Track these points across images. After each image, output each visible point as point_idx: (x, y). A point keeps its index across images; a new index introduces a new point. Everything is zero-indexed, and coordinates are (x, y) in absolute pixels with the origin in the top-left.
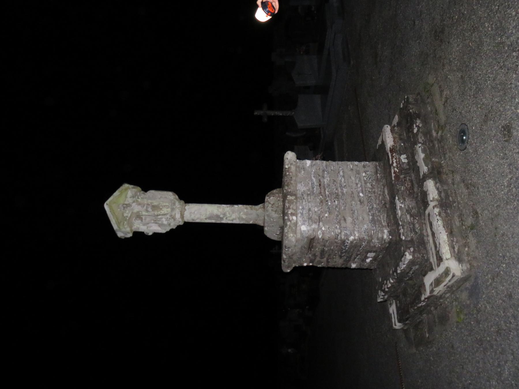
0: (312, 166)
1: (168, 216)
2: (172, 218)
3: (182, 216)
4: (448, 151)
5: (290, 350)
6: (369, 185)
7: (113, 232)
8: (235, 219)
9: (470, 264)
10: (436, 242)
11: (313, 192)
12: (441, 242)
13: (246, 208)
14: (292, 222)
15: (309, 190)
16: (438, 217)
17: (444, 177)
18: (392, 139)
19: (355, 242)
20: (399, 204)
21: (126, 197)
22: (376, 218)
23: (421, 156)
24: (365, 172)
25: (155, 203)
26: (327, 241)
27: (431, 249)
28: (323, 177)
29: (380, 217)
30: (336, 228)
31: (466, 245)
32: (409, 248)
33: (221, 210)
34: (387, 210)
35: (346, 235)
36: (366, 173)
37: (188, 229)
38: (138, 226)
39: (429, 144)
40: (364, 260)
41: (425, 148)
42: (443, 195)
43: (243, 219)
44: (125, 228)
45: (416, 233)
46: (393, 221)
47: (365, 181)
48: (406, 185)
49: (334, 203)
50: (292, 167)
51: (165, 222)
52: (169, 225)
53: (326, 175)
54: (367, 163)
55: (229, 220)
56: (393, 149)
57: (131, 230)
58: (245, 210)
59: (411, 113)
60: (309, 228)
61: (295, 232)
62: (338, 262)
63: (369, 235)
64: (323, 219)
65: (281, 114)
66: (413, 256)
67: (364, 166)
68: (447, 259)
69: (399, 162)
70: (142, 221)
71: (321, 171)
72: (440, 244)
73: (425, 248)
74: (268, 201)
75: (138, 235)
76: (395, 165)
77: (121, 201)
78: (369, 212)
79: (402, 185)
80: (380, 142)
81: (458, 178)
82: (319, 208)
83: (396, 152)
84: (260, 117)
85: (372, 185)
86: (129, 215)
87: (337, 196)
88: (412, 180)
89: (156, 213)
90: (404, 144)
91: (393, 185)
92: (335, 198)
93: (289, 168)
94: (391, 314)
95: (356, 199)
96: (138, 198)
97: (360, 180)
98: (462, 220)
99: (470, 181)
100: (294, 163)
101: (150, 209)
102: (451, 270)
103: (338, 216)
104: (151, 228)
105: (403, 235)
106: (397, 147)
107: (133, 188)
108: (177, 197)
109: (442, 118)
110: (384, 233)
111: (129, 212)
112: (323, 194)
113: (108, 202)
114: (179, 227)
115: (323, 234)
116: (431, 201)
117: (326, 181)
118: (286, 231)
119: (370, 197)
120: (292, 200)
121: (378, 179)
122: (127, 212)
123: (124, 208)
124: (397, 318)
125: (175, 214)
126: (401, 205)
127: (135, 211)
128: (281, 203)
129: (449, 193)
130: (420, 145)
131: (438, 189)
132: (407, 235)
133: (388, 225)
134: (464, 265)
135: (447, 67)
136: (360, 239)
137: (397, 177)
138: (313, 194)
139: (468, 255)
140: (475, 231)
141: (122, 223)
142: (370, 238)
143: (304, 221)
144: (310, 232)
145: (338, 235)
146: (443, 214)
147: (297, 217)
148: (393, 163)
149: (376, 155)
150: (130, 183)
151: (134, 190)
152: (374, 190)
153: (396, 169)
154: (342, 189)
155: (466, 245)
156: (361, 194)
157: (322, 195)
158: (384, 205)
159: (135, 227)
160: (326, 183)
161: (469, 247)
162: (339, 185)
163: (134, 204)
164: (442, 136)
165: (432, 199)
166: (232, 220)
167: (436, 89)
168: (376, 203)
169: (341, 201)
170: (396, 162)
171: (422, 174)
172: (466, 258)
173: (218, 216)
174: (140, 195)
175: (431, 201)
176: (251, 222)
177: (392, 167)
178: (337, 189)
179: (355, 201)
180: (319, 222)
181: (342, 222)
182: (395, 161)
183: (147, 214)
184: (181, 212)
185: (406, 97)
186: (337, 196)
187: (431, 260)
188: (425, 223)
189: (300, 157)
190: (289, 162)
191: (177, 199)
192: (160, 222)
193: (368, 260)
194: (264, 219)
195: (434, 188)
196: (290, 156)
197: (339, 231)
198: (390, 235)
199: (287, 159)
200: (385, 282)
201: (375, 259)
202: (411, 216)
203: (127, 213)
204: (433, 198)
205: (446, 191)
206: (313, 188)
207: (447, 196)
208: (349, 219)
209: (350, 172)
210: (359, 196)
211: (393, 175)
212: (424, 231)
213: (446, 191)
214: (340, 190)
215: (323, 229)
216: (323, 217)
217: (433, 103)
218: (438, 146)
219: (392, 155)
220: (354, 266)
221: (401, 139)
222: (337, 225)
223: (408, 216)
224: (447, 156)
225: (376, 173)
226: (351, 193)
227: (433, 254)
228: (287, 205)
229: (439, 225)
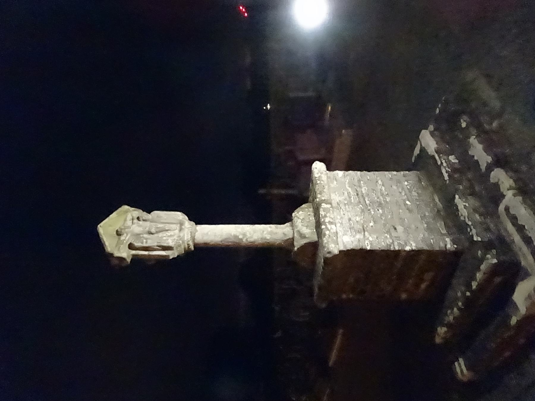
0: (344, 176)
1: (175, 237)
6: (414, 194)
14: (332, 231)
15: (345, 199)
28: (360, 187)
36: (408, 182)
37: (201, 253)
50: (322, 175)
54: (407, 172)
60: (353, 239)
67: (404, 176)
69: (448, 162)
76: (445, 164)
80: (417, 151)
87: (380, 205)
93: (319, 176)
115: (371, 244)
118: (326, 241)
120: (328, 208)
125: (184, 235)
126: (464, 204)
148: (442, 163)
153: (447, 169)
156: (408, 202)
160: (364, 192)
162: (379, 194)
170: (446, 162)
171: (483, 167)
177: (442, 167)
180: (364, 232)
181: (392, 230)
182: (444, 161)
189: (330, 168)
190: (319, 171)
196: (318, 167)
197: (391, 241)
198: (454, 244)
202: (480, 215)
204: (510, 186)
206: (350, 197)
208: (400, 229)
210: (406, 204)
215: (371, 239)
216: (367, 226)
222: (386, 235)
225: (420, 180)
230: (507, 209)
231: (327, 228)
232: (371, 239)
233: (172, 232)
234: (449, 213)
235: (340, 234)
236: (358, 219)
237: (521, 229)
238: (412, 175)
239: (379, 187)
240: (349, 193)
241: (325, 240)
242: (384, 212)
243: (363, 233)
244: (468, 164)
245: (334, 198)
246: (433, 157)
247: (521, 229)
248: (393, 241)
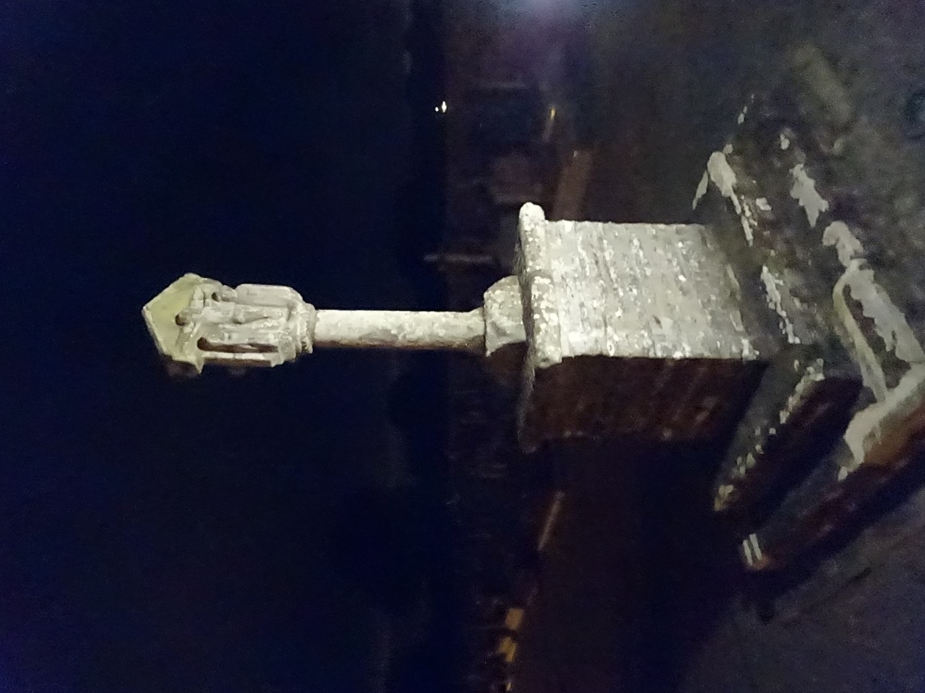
15: (576, 271)
28: (602, 250)
30: (643, 336)
37: (325, 358)
47: (684, 256)
49: (630, 293)
60: (585, 338)
64: (613, 321)
66: (825, 375)
76: (748, 214)
80: (702, 190)
85: (699, 262)
87: (635, 281)
93: (532, 230)
97: (675, 254)
113: (149, 304)
115: (617, 347)
133: (747, 331)
138: (586, 277)
148: (743, 212)
153: (752, 221)
154: (642, 269)
160: (608, 258)
162: (634, 262)
173: (386, 331)
180: (606, 326)
181: (653, 324)
182: (746, 208)
190: (532, 221)
197: (650, 343)
198: (755, 348)
202: (802, 301)
206: (583, 268)
208: (666, 322)
210: (678, 282)
216: (611, 317)
219: (739, 199)
222: (643, 332)
223: (797, 302)
230: (847, 290)
232: (616, 338)
233: (276, 321)
235: (564, 329)
240: (582, 260)
241: (539, 339)
242: (640, 293)
243: (603, 328)
244: (787, 213)
246: (729, 201)
247: (866, 325)
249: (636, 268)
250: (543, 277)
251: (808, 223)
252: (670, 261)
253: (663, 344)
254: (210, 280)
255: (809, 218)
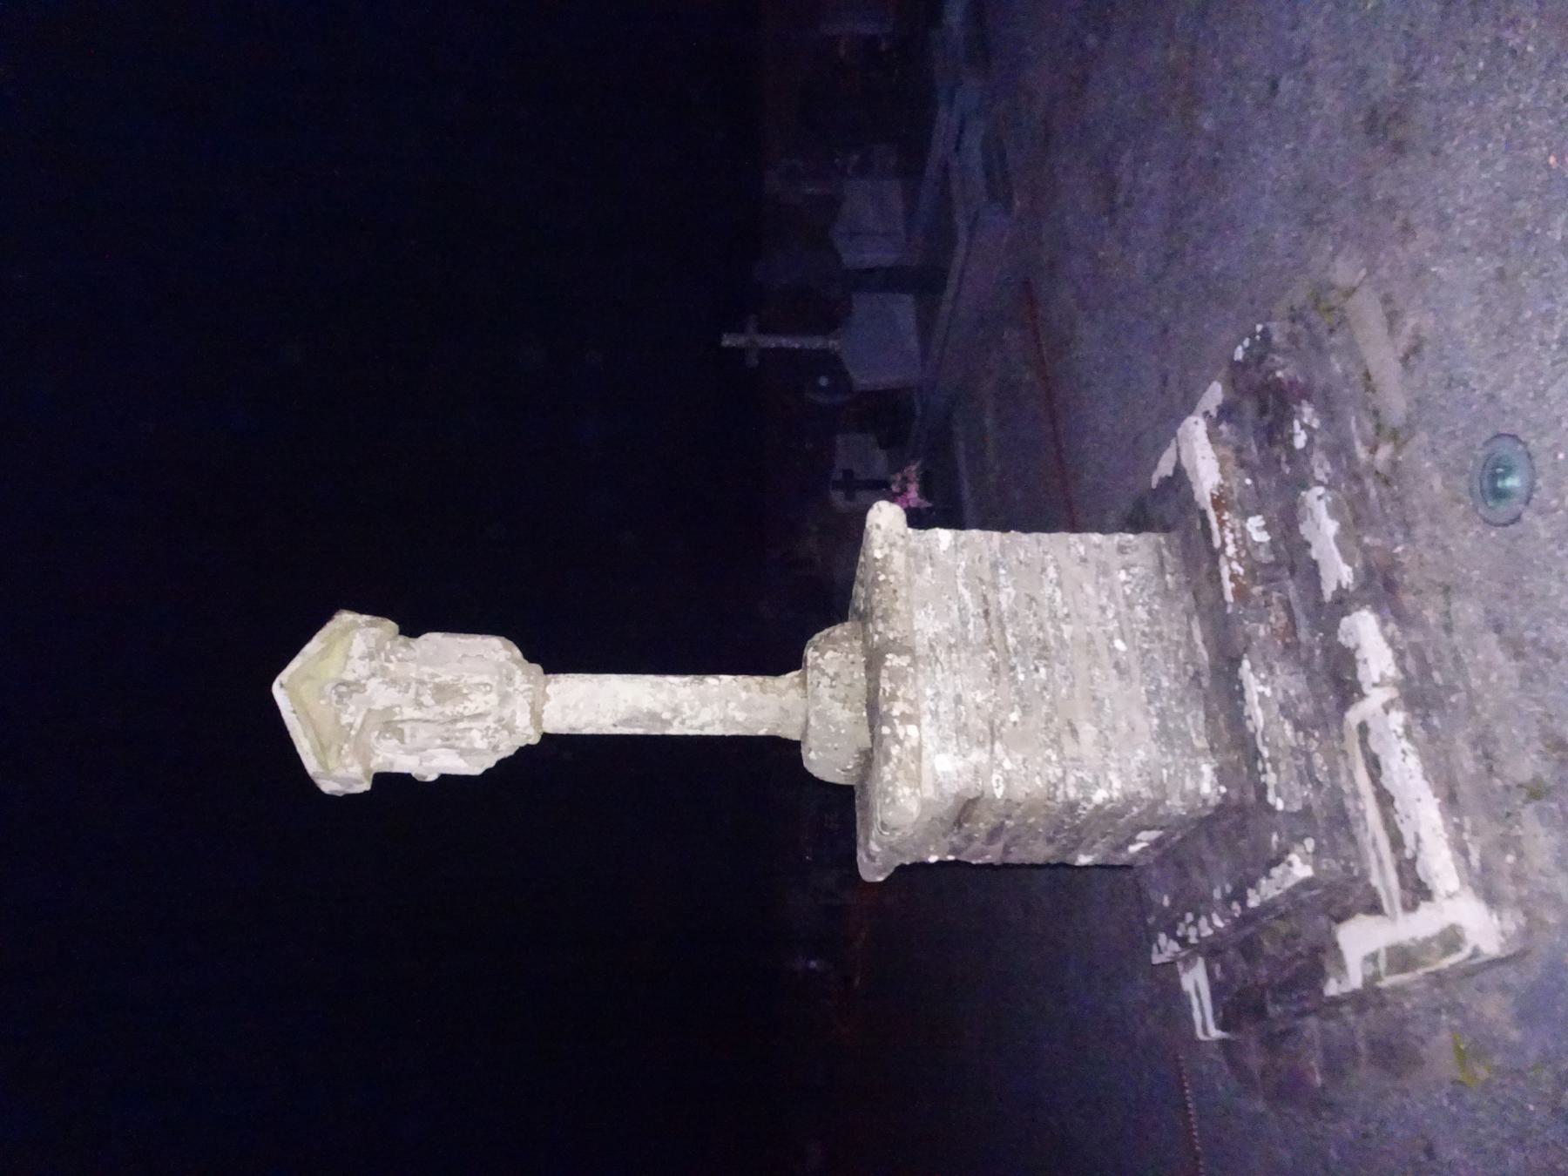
0: (956, 548)
1: (490, 721)
2: (504, 727)
3: (536, 717)
4: (1421, 516)
5: (813, 964)
6: (1141, 613)
7: (306, 783)
8: (713, 723)
9: (1526, 913)
10: (1403, 828)
11: (965, 638)
12: (1423, 834)
13: (747, 688)
14: (907, 744)
15: (951, 631)
16: (1405, 744)
17: (1408, 600)
18: (1215, 465)
19: (1108, 806)
20: (1255, 686)
21: (348, 657)
22: (1171, 725)
23: (1323, 528)
24: (1126, 567)
25: (446, 678)
26: (1019, 804)
27: (1374, 844)
28: (995, 587)
29: (1184, 719)
30: (1048, 760)
31: (1507, 843)
32: (1300, 840)
33: (663, 696)
34: (1206, 697)
35: (1081, 784)
36: (1128, 574)
37: (555, 761)
38: (390, 756)
39: (1349, 488)
40: (1121, 848)
41: (1336, 502)
42: (1410, 663)
43: (736, 723)
44: (345, 767)
45: (1318, 785)
46: (1227, 737)
47: (1126, 597)
48: (1272, 619)
49: (1035, 676)
50: (896, 553)
51: (481, 744)
52: (495, 748)
53: (1002, 580)
54: (1131, 536)
55: (691, 727)
56: (1220, 497)
57: (366, 771)
58: (744, 695)
59: (1279, 379)
60: (960, 764)
61: (916, 781)
62: (1041, 852)
63: (1157, 782)
64: (1003, 730)
65: (797, 346)
66: (1316, 867)
67: (1122, 549)
68: (1450, 896)
69: (1243, 541)
70: (402, 741)
71: (987, 564)
72: (1418, 840)
73: (1352, 839)
74: (816, 667)
75: (390, 785)
76: (1231, 550)
77: (331, 670)
78: (1150, 702)
79: (1260, 620)
80: (1165, 467)
81: (1469, 612)
82: (979, 688)
83: (1228, 507)
84: (740, 352)
85: (1150, 613)
86: (359, 721)
87: (1044, 652)
88: (1289, 603)
89: (449, 710)
90: (1254, 479)
91: (1227, 621)
92: (1039, 657)
93: (886, 557)
94: (1187, 997)
95: (1105, 658)
96: (388, 660)
97: (1111, 595)
98: (1487, 756)
99: (1530, 635)
100: (901, 542)
101: (427, 699)
102: (1468, 936)
103: (1049, 720)
104: (435, 763)
105: (1278, 794)
106: (1231, 490)
107: (371, 625)
108: (518, 653)
109: (1396, 404)
110: (1200, 774)
111: (358, 710)
112: (1004, 646)
113: (283, 677)
114: (525, 752)
115: (1008, 782)
116: (1375, 685)
117: (1006, 598)
118: (888, 777)
119: (1148, 651)
120: (901, 668)
121: (1167, 589)
122: (352, 708)
123: (340, 696)
124: (1215, 1014)
125: (514, 713)
126: (1261, 689)
127: (378, 706)
128: (860, 674)
129: (1431, 659)
130: (1320, 490)
131: (1391, 642)
132: (1291, 794)
133: (1212, 749)
134: (1507, 915)
135: (1425, 236)
136: (1125, 796)
137: (1240, 593)
138: (967, 644)
139: (1518, 878)
140: (1554, 806)
141: (334, 748)
142: (1158, 795)
143: (945, 739)
144: (968, 777)
145: (1056, 786)
146: (1420, 733)
147: (919, 726)
148: (1224, 545)
149: (1160, 509)
150: (361, 610)
151: (373, 630)
152: (1157, 628)
153: (1235, 565)
154: (1059, 629)
155: (1507, 843)
156: (1119, 644)
157: (994, 649)
158: (1193, 679)
159: (380, 760)
160: (1004, 606)
161: (1520, 855)
162: (1045, 614)
163: (373, 684)
164: (1395, 464)
165: (1376, 679)
166: (702, 728)
167: (1367, 311)
168: (1166, 674)
169: (1057, 666)
170: (1235, 541)
172: (1509, 890)
173: (654, 716)
174: (393, 652)
175: (1375, 685)
176: (762, 732)
177: (1222, 560)
178: (1041, 627)
179: (1101, 667)
180: (993, 743)
181: (1066, 739)
182: (1229, 538)
183: (417, 714)
184: (532, 705)
185: (1259, 328)
186: (1044, 652)
187: (1375, 881)
188: (1344, 752)
191: (516, 662)
192: (463, 744)
193: (1133, 849)
194: (807, 722)
195: (1380, 639)
199: (878, 527)
200: (1189, 917)
201: (1157, 844)
202: (1298, 726)
203: (352, 715)
204: (1382, 676)
205: (1419, 652)
206: (965, 624)
207: (1425, 670)
208: (1088, 731)
209: (1079, 568)
210: (1112, 651)
211: (1228, 586)
212: (1343, 778)
213: (1419, 652)
214: (1051, 631)
215: (1007, 765)
216: (1002, 724)
217: (1352, 350)
218: (1379, 495)
219: (1219, 517)
220: (1083, 860)
221: (1242, 464)
222: (1049, 752)
224: (1419, 532)
225: (1161, 568)
226: (1085, 638)
227: (1380, 862)
228: (886, 685)
229: (1405, 768)
230: (1363, 728)
231: (894, 735)
232: (1007, 765)
234: (1221, 688)
235: (929, 748)
236: (980, 698)
237: (1385, 799)
238: (1142, 546)
239: (1048, 590)
240: (962, 609)
241: (887, 772)
242: (1050, 675)
243: (988, 748)
244: (1291, 557)
245: (921, 626)
246: (1203, 513)
248: (1065, 772)
249: (1048, 625)
250: (898, 654)
251: (1320, 592)
252: (1103, 609)
253: (1079, 774)
254: (375, 619)
255: (1323, 587)
